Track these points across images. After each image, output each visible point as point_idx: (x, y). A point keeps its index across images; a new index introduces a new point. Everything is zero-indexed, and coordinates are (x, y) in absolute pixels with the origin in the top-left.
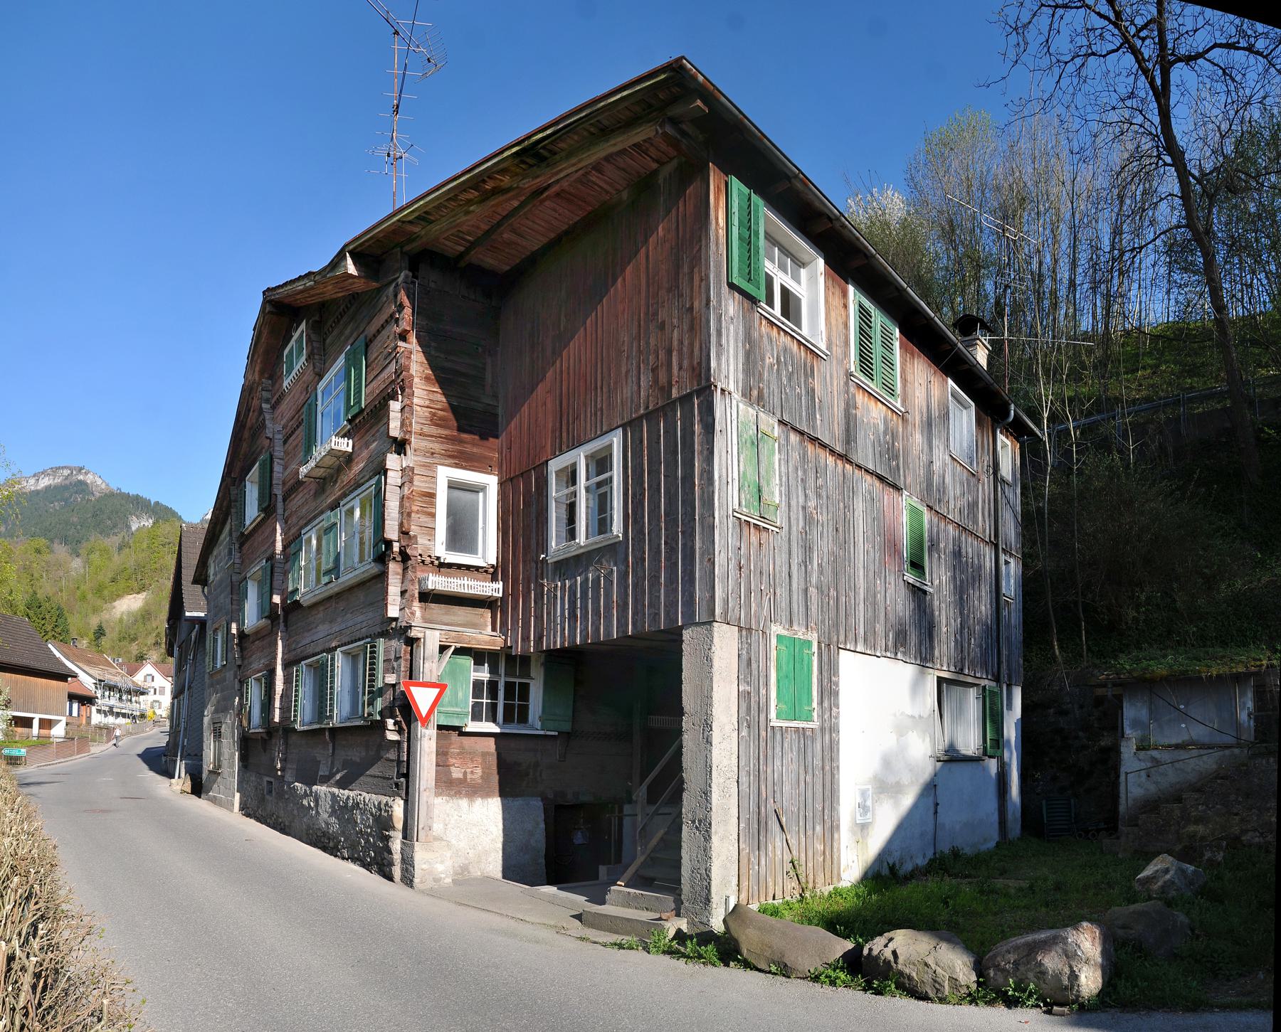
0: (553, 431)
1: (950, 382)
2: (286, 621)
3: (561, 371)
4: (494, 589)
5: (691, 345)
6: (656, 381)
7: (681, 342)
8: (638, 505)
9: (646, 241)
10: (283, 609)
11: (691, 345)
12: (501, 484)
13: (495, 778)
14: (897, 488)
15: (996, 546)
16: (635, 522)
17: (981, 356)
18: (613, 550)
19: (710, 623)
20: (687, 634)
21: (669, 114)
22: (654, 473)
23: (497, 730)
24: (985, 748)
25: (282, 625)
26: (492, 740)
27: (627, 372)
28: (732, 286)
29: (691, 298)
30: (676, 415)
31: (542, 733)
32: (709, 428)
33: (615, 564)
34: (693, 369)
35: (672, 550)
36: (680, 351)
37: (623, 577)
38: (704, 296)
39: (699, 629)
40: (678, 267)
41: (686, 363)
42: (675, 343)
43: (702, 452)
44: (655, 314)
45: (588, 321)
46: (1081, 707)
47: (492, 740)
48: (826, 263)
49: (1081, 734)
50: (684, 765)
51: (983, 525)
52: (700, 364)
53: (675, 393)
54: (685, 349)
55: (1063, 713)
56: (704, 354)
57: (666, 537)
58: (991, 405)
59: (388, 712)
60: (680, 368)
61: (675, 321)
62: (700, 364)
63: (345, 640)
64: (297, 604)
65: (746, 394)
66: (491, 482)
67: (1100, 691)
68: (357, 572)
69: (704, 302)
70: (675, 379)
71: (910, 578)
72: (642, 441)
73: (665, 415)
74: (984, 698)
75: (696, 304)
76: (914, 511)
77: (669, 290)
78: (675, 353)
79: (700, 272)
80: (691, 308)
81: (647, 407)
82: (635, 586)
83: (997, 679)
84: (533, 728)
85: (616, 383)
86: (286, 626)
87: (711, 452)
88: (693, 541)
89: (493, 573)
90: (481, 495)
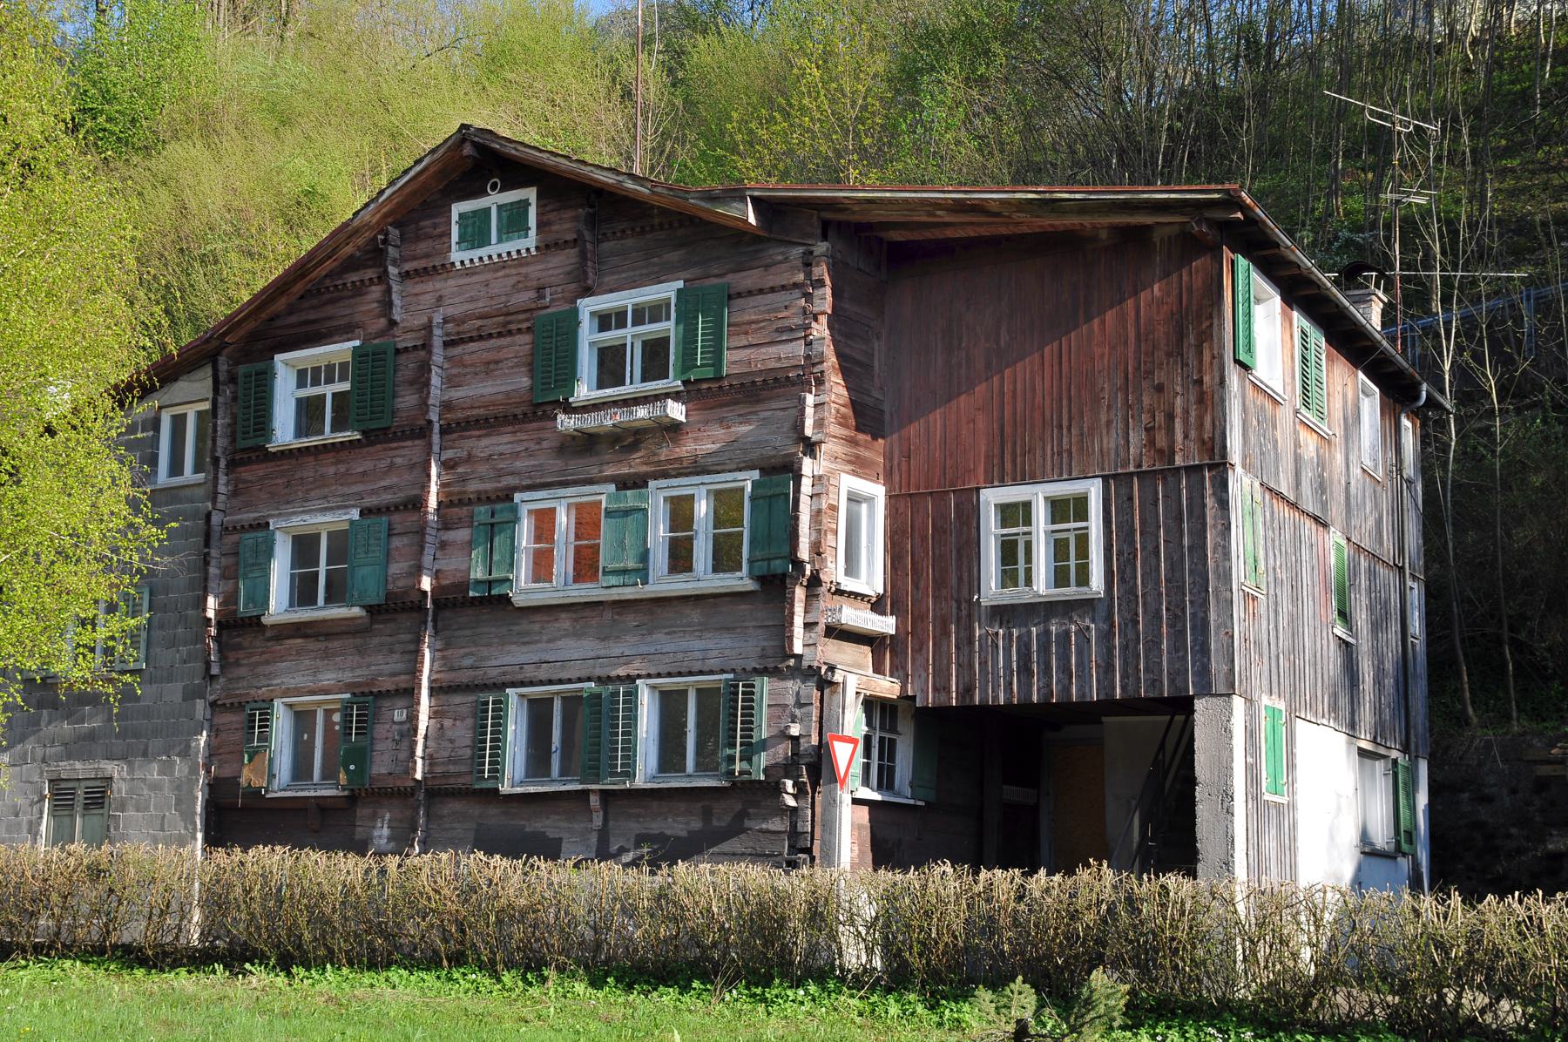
0: (987, 457)
1: (1361, 375)
2: (435, 620)
3: (1002, 394)
4: (886, 624)
5: (1200, 418)
6: (1151, 442)
7: (1186, 411)
8: (1128, 562)
9: (1136, 293)
10: (434, 601)
11: (1200, 418)
12: (891, 498)
13: (870, 855)
14: (1325, 525)
15: (1401, 569)
16: (1122, 580)
17: (1373, 316)
18: (1088, 605)
19: (1229, 695)
20: (1199, 704)
21: (1206, 215)
22: (1149, 531)
23: (877, 796)
24: (1398, 843)
25: (430, 624)
26: (866, 809)
27: (1109, 423)
28: (1237, 361)
29: (1200, 371)
30: (1180, 482)
31: (912, 802)
32: (1224, 504)
33: (1093, 621)
34: (1203, 442)
35: (1177, 618)
36: (1186, 421)
37: (1106, 637)
38: (1217, 374)
39: (1214, 700)
40: (1181, 336)
41: (1193, 434)
42: (1178, 411)
43: (1214, 526)
44: (1150, 373)
45: (1047, 350)
46: (1514, 791)
47: (866, 809)
48: (1283, 299)
49: (1513, 831)
50: (1198, 836)
51: (1388, 549)
52: (1212, 439)
53: (1179, 461)
54: (1192, 420)
55: (1488, 800)
56: (1217, 433)
57: (1168, 603)
58: (1398, 392)
59: (789, 767)
60: (1186, 437)
61: (1179, 389)
62: (1212, 439)
63: (663, 669)
64: (505, 600)
65: (1244, 466)
66: (878, 491)
67: (1544, 770)
68: (701, 584)
69: (1217, 380)
70: (1178, 446)
71: (1340, 631)
72: (1131, 499)
73: (1164, 479)
74: (1395, 776)
75: (1207, 379)
76: (1339, 548)
77: (1169, 355)
78: (1177, 420)
79: (1211, 349)
80: (1200, 382)
81: (1140, 466)
82: (1124, 648)
83: (1405, 749)
84: (899, 794)
85: (1091, 429)
86: (435, 627)
87: (1227, 527)
88: (1206, 612)
89: (877, 606)
90: (864, 506)
